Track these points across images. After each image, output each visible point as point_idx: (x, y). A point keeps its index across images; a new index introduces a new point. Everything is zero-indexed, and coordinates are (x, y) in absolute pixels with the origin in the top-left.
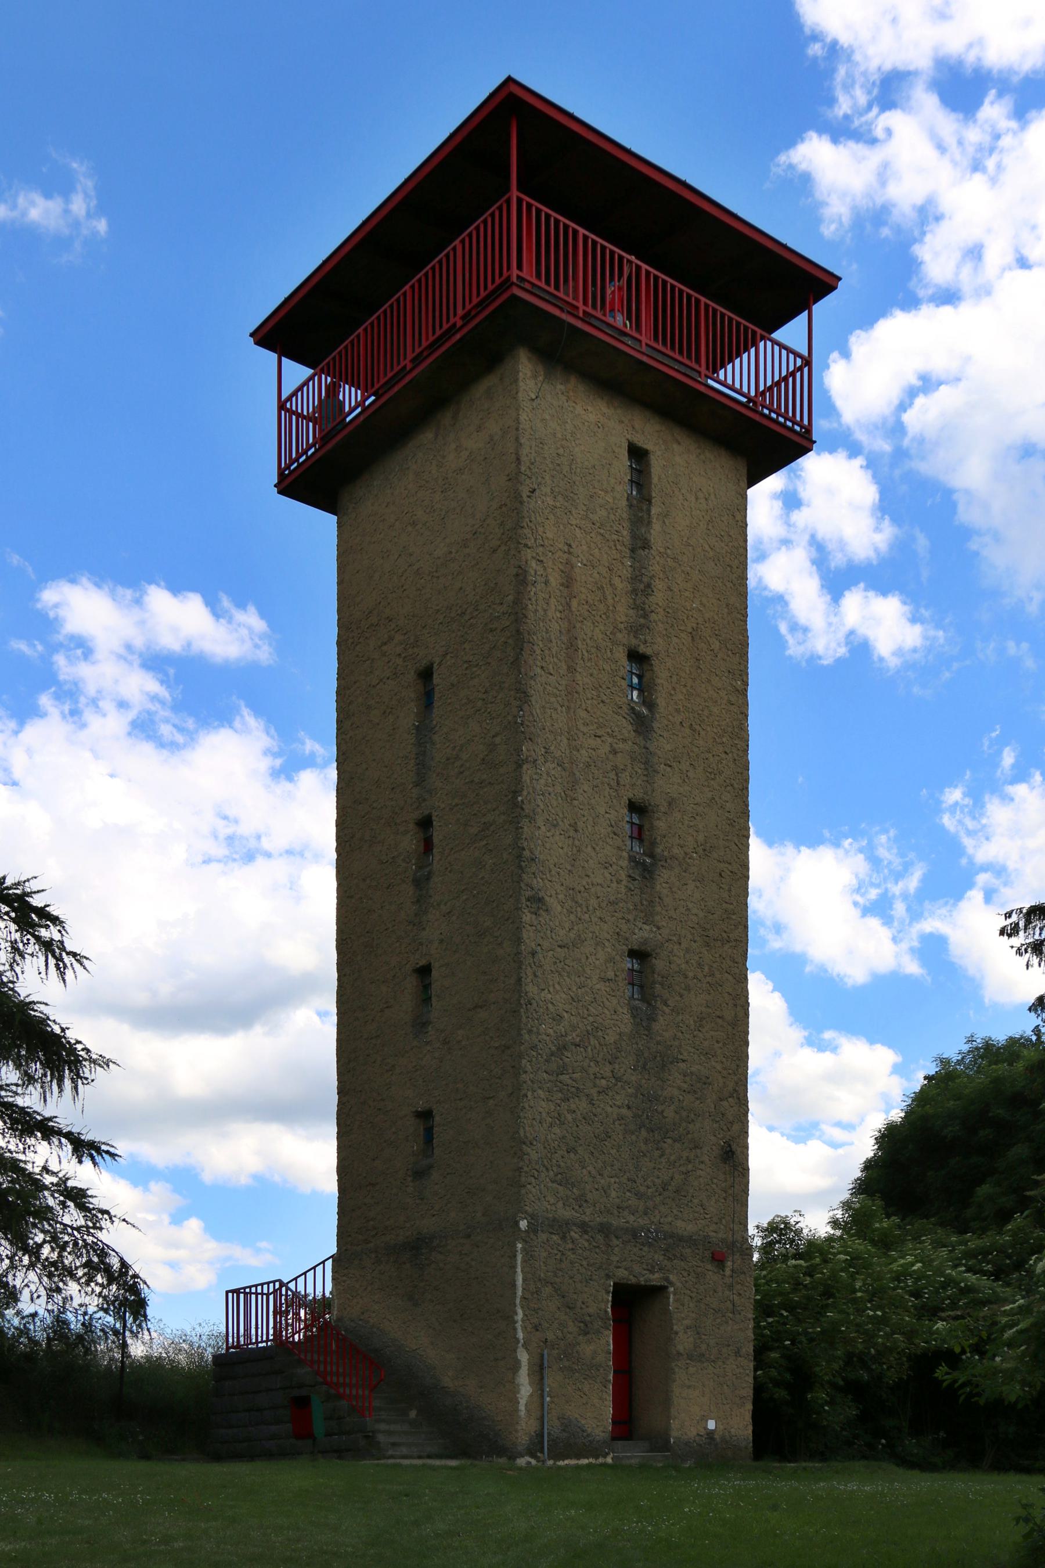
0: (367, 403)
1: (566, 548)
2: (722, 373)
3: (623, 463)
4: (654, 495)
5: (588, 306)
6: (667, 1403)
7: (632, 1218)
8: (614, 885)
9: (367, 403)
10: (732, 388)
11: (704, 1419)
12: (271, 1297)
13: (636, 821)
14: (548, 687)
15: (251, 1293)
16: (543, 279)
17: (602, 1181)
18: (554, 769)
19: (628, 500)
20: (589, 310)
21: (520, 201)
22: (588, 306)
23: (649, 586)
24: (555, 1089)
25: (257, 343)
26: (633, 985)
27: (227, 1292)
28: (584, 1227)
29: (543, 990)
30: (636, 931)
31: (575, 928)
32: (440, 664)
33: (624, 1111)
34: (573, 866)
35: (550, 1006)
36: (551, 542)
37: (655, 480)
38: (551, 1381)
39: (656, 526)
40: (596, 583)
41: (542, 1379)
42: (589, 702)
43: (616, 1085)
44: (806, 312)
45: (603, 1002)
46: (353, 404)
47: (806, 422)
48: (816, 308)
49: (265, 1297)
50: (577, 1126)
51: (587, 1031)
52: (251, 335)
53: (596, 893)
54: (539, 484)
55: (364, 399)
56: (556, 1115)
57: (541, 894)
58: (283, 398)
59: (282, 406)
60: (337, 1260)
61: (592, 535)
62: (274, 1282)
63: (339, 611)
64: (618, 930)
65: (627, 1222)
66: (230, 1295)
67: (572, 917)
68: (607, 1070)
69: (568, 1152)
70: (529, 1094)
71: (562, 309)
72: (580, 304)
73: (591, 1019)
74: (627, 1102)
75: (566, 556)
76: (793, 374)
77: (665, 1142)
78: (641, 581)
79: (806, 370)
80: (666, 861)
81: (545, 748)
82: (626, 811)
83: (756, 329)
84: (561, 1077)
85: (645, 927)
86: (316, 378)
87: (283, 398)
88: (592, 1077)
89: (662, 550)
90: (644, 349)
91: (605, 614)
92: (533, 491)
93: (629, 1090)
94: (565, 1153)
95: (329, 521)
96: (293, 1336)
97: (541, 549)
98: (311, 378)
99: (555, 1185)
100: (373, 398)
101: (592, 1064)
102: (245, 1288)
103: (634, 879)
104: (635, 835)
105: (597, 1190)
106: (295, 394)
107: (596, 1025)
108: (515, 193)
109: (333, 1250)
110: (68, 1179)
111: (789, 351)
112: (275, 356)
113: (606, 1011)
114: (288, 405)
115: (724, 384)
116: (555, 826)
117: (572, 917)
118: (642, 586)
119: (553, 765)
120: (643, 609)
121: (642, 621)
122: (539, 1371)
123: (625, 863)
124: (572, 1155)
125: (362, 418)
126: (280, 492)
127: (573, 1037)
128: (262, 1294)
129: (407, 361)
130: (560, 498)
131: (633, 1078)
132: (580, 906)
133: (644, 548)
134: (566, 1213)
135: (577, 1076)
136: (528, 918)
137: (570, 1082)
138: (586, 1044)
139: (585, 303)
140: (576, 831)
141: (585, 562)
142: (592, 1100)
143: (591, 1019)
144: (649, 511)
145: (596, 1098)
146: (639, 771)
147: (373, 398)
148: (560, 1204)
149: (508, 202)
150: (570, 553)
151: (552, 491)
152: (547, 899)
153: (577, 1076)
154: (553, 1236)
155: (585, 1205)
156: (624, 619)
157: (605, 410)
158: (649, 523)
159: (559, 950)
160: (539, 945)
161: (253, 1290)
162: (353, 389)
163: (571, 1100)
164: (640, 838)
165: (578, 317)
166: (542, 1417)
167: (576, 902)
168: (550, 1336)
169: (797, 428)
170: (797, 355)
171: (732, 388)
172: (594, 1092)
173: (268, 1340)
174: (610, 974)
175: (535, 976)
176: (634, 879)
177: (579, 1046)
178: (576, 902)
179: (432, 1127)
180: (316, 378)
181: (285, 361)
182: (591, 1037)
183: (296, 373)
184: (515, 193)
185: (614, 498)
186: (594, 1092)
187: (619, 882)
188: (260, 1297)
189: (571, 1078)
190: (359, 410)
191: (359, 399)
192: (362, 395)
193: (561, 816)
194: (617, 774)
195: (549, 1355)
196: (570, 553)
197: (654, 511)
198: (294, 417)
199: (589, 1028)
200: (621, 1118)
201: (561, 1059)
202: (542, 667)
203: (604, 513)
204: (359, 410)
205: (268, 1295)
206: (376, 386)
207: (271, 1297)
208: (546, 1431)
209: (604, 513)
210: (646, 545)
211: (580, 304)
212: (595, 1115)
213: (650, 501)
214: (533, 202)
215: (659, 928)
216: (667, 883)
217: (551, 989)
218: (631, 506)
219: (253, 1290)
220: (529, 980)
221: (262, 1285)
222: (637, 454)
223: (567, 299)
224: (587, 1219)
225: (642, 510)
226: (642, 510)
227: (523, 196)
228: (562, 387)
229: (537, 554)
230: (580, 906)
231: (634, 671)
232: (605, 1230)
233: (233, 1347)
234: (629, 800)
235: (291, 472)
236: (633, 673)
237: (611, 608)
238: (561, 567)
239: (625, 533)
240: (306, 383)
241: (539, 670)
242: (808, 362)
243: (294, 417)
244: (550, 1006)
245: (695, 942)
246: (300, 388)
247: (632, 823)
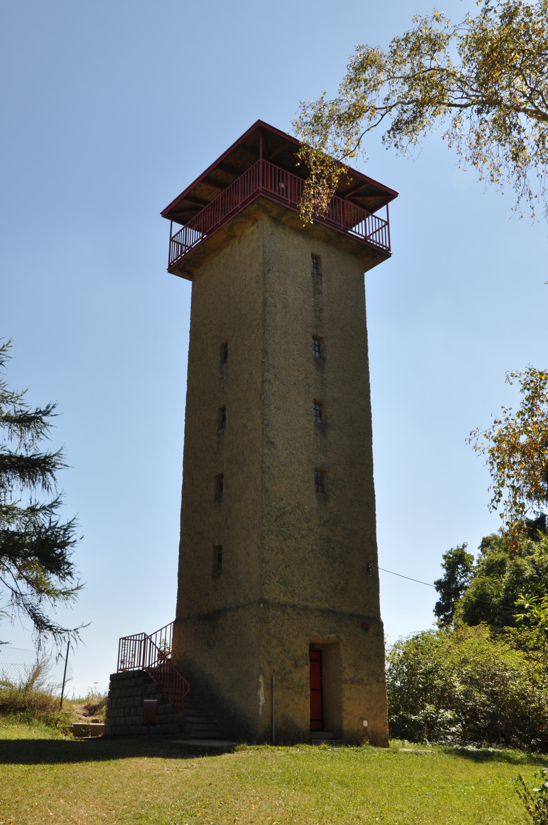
0: (204, 237)
1: (284, 293)
2: (354, 229)
3: (309, 261)
4: (323, 272)
5: (264, 187)
6: (340, 709)
7: (319, 604)
8: (308, 437)
9: (204, 237)
10: (358, 234)
11: (362, 719)
12: (143, 642)
13: (318, 408)
14: (276, 349)
15: (131, 640)
16: (265, 186)
17: (304, 583)
18: (279, 384)
19: (312, 274)
20: (293, 202)
21: (263, 162)
22: (264, 187)
23: (322, 309)
24: (279, 535)
25: (163, 216)
26: (318, 484)
27: (120, 639)
28: (294, 607)
29: (274, 486)
30: (319, 459)
31: (289, 457)
32: (230, 340)
33: (314, 547)
34: (288, 428)
35: (277, 493)
36: (278, 290)
37: (323, 267)
38: (278, 694)
39: (325, 285)
40: (298, 307)
41: (272, 693)
42: (295, 356)
43: (309, 533)
44: (386, 206)
45: (303, 492)
46: (198, 238)
47: (388, 246)
48: (390, 204)
49: (134, 641)
50: (291, 554)
51: (295, 506)
52: (161, 213)
53: (299, 441)
54: (273, 267)
55: (202, 236)
56: (280, 548)
57: (273, 440)
58: (172, 236)
59: (171, 239)
60: (175, 623)
61: (296, 288)
62: (142, 634)
63: (191, 319)
64: (310, 458)
65: (317, 605)
66: (121, 640)
67: (288, 452)
68: (305, 526)
69: (286, 567)
70: (266, 537)
71: (281, 201)
72: (289, 200)
73: (297, 500)
74: (315, 542)
75: (285, 296)
76: (381, 228)
77: (335, 564)
78: (318, 307)
79: (387, 226)
80: (332, 427)
81: (274, 375)
82: (313, 404)
83: (340, 198)
84: (282, 529)
85: (323, 457)
86: (185, 229)
87: (172, 236)
88: (298, 529)
89: (327, 295)
90: (342, 229)
91: (302, 320)
92: (270, 270)
93: (317, 537)
94: (284, 568)
95: (190, 283)
96: (151, 665)
97: (273, 293)
98: (183, 229)
99: (279, 584)
100: (206, 236)
101: (297, 522)
102: (128, 637)
103: (317, 435)
104: (318, 414)
105: (301, 588)
106: (176, 235)
107: (299, 503)
108: (261, 159)
109: (173, 618)
110: (71, 575)
111: (379, 219)
112: (170, 221)
113: (304, 497)
114: (174, 239)
115: (355, 232)
116: (279, 410)
117: (288, 452)
118: (319, 309)
119: (278, 383)
120: (319, 318)
121: (319, 323)
122: (270, 688)
123: (312, 427)
124: (288, 569)
125: (201, 243)
126: (169, 272)
127: (288, 508)
128: (133, 640)
129: (219, 221)
130: (281, 273)
131: (319, 530)
132: (292, 446)
133: (319, 294)
134: (284, 599)
135: (290, 528)
136: (266, 451)
137: (286, 531)
138: (295, 513)
139: (291, 199)
140: (289, 412)
141: (293, 298)
142: (298, 541)
143: (297, 500)
144: (321, 279)
145: (300, 540)
146: (319, 387)
147: (206, 236)
148: (282, 595)
149: (259, 163)
150: (286, 295)
151: (278, 270)
152: (275, 442)
153: (290, 528)
154: (278, 612)
155: (294, 596)
156: (310, 322)
157: (301, 240)
158: (321, 284)
159: (281, 467)
160: (271, 464)
161: (129, 638)
162: (199, 233)
163: (287, 541)
164: (320, 416)
165: (288, 205)
166: (272, 717)
167: (290, 445)
168: (276, 668)
169: (384, 248)
170: (382, 220)
171: (358, 234)
172: (298, 537)
173: (140, 666)
174: (306, 479)
175: (270, 479)
176: (317, 435)
177: (291, 513)
178: (290, 445)
179: (222, 553)
180: (185, 229)
181: (173, 223)
182: (297, 510)
183: (177, 227)
184: (261, 159)
185: (306, 274)
186: (298, 537)
187: (310, 436)
188: (137, 642)
189: (287, 529)
190: (201, 240)
191: (201, 236)
192: (202, 234)
193: (282, 405)
194: (308, 387)
195: (276, 679)
196: (286, 295)
197: (323, 279)
198: (180, 245)
199: (296, 505)
200: (313, 550)
201: (282, 520)
202: (273, 341)
203: (301, 279)
204: (201, 240)
205: (141, 641)
206: (207, 231)
207: (143, 642)
208: (274, 725)
209: (301, 279)
210: (320, 292)
211: (289, 200)
212: (299, 549)
213: (321, 276)
214: (276, 167)
215: (330, 458)
216: (333, 437)
217: (278, 486)
218: (313, 277)
219: (129, 638)
220: (266, 481)
221: (133, 636)
222: (315, 258)
223: (275, 194)
224: (296, 604)
225: (318, 278)
226: (318, 278)
227: (264, 161)
228: (283, 231)
229: (272, 295)
230: (292, 446)
231: (316, 344)
232: (305, 609)
233: (120, 670)
234: (314, 399)
235: (174, 264)
236: (315, 345)
237: (305, 317)
238: (282, 300)
239: (311, 287)
240: (181, 231)
241: (271, 342)
242: (387, 223)
243: (180, 245)
244: (277, 493)
245: (347, 465)
246: (179, 233)
247: (316, 410)
